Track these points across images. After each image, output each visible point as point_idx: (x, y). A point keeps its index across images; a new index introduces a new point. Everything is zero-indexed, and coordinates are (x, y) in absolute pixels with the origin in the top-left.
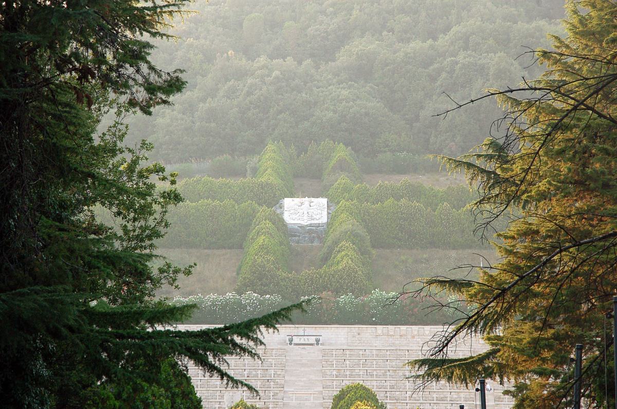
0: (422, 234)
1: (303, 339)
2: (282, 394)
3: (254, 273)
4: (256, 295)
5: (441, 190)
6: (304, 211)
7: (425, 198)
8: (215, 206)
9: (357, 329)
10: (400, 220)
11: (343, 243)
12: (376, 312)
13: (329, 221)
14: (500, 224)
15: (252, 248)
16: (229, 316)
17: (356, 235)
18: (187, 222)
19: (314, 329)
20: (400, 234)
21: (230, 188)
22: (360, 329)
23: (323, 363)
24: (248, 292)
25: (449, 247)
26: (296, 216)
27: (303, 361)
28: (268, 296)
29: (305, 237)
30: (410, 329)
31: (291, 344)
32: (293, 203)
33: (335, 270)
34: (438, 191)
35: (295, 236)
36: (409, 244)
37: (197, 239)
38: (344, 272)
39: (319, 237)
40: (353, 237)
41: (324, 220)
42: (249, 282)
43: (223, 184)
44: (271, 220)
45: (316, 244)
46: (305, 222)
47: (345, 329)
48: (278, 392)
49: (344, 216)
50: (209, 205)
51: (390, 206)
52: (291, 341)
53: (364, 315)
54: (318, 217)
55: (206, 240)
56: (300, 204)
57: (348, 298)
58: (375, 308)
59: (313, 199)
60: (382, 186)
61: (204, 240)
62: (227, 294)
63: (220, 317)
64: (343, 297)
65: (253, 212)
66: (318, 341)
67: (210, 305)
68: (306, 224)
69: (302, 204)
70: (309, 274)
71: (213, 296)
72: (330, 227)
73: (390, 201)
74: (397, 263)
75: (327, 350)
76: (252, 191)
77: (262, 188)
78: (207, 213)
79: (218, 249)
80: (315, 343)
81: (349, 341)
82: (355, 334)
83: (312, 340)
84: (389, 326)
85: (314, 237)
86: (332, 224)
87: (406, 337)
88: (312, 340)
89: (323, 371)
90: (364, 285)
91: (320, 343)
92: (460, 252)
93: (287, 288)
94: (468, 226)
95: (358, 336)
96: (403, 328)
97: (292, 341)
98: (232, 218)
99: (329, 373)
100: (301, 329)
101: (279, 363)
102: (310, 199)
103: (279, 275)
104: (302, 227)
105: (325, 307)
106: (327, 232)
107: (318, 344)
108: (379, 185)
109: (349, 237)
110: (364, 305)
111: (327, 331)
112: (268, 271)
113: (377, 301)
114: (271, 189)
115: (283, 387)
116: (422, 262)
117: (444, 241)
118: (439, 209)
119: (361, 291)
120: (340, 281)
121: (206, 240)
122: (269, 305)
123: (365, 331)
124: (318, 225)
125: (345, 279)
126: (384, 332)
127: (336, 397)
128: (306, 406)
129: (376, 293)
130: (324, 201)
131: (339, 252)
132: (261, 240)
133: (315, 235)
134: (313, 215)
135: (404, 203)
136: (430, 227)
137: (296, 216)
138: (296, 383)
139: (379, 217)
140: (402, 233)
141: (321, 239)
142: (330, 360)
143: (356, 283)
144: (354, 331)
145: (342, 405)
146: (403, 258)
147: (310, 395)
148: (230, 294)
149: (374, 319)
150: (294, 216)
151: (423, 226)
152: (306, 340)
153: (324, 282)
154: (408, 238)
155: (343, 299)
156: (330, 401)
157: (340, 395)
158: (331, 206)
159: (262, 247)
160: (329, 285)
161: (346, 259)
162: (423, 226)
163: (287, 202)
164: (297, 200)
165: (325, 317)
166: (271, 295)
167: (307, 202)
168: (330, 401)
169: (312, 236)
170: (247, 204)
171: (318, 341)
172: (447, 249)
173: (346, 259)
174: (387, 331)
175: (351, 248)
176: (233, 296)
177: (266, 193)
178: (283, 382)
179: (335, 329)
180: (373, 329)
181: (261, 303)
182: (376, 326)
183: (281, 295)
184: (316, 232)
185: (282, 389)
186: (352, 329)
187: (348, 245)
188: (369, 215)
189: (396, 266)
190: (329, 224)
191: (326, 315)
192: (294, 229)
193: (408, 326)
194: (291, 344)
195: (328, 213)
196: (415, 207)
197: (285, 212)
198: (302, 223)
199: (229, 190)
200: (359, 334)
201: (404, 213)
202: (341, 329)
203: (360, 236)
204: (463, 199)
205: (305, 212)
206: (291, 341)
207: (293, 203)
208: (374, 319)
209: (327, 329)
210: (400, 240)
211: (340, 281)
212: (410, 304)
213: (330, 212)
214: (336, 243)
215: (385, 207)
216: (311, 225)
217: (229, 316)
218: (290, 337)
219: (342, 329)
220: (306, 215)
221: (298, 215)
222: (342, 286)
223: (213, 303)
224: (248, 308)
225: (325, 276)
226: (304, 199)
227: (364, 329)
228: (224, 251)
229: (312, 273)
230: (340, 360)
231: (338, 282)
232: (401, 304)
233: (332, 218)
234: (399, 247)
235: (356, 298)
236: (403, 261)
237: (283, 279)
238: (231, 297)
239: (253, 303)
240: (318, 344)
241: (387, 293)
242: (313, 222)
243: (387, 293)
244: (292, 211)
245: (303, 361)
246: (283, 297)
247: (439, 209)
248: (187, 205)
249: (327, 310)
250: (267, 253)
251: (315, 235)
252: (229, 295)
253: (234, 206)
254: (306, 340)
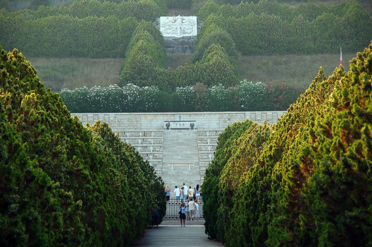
0: (280, 42)
1: (178, 125)
2: (161, 166)
3: (134, 68)
4: (136, 86)
5: (294, 8)
6: (177, 27)
7: (281, 15)
8: (100, 21)
9: (228, 115)
10: (260, 30)
11: (213, 45)
12: (245, 100)
13: (199, 34)
14: (348, 31)
15: (132, 52)
16: (112, 105)
17: (224, 39)
18: (76, 35)
19: (188, 115)
20: (261, 43)
21: (113, 9)
22: (230, 115)
23: (198, 141)
24: (129, 84)
25: (304, 53)
26: (170, 31)
27: (179, 141)
28: (147, 87)
29: (179, 48)
30: (275, 114)
31: (168, 129)
32: (167, 20)
33: (207, 65)
34: (292, 9)
35: (170, 47)
36: (269, 51)
37: (86, 50)
38: (215, 66)
39: (190, 48)
40: (221, 40)
41: (195, 33)
42: (129, 76)
43: (107, 6)
44: (148, 31)
45: (188, 53)
46: (178, 35)
47: (216, 115)
48: (157, 163)
49: (212, 26)
50: (95, 20)
51: (252, 19)
52: (168, 126)
53: (234, 103)
54: (189, 31)
55: (93, 51)
56: (174, 21)
57: (219, 88)
58: (243, 96)
59: (184, 17)
60: (243, 6)
61: (91, 51)
62: (110, 86)
63: (104, 106)
64: (214, 87)
65: (134, 26)
66: (192, 126)
67: (95, 95)
68: (179, 37)
69: (175, 21)
70: (183, 69)
71: (97, 88)
72: (200, 37)
73: (252, 15)
74: (259, 65)
75: (201, 132)
76: (132, 11)
77: (141, 9)
78: (93, 27)
79: (103, 58)
80: (190, 127)
81: (220, 126)
82: (226, 119)
83: (187, 125)
84: (256, 112)
85: (186, 48)
86: (202, 34)
87: (272, 121)
88: (187, 125)
89: (199, 147)
90: (232, 78)
91: (194, 127)
92: (314, 56)
93: (163, 82)
94: (320, 35)
95: (228, 122)
96: (269, 113)
97: (169, 126)
98: (115, 31)
99: (204, 149)
100: (177, 115)
101: (158, 142)
102: (182, 17)
103: (157, 71)
104: (176, 39)
105: (198, 96)
106: (197, 43)
107: (192, 128)
108: (241, 5)
109: (218, 41)
110: (233, 94)
111: (201, 117)
112: (146, 67)
113: (246, 90)
114: (149, 9)
115: (162, 159)
116: (281, 64)
117: (299, 48)
118: (294, 21)
119: (230, 83)
120: (211, 74)
121: (93, 51)
122: (147, 95)
123: (235, 117)
124: (190, 38)
125: (215, 73)
126: (252, 116)
127: (221, 135)
128: (184, 174)
129: (244, 83)
130: (194, 18)
131: (209, 52)
132: (140, 43)
133: (187, 46)
134: (185, 30)
135: (264, 17)
136: (287, 36)
137: (170, 31)
138: (173, 157)
139: (243, 29)
140: (262, 42)
141: (192, 49)
142: (204, 139)
143: (226, 76)
144: (225, 117)
145: (229, 142)
146: (264, 61)
147: (187, 165)
148: (112, 86)
149: (243, 106)
150: (169, 31)
151: (281, 35)
152: (182, 125)
153: (197, 75)
154: (268, 46)
155: (213, 89)
156: (216, 137)
157: (226, 134)
158: (200, 23)
159: (141, 49)
160: (201, 79)
161: (216, 56)
162: (281, 35)
163: (163, 20)
164: (171, 18)
165: (198, 105)
166: (150, 86)
167: (180, 19)
168: (216, 137)
169: (184, 47)
170: (128, 19)
171: (192, 126)
172: (302, 55)
173: (216, 56)
174: (254, 117)
175: (220, 49)
176: (115, 88)
177: (144, 13)
178: (161, 156)
179: (208, 115)
180: (242, 115)
181: (141, 93)
182: (244, 112)
183: (159, 87)
184: (186, 43)
185: (161, 160)
186: (223, 115)
187: (217, 46)
188: (233, 27)
189: (258, 68)
190: (199, 36)
191: (199, 104)
192: (169, 41)
193: (274, 112)
194: (168, 129)
195: (198, 28)
196: (273, 19)
197: (161, 28)
198: (176, 36)
199: (113, 10)
200: (229, 120)
201: (264, 25)
202: (213, 115)
203: (228, 40)
204: (313, 15)
205: (178, 27)
206: (168, 126)
207: (167, 20)
208: (243, 106)
209: (200, 115)
210: (261, 48)
211: (211, 74)
212: (275, 92)
213: (200, 27)
214: (206, 46)
215: (248, 20)
216: (183, 38)
217: (112, 105)
218: (167, 123)
219: (214, 115)
220: (179, 30)
221: (172, 30)
222: (213, 79)
223: (97, 94)
224: (129, 98)
225: (198, 71)
226: (177, 17)
227: (234, 115)
228: (108, 59)
229: (186, 68)
230: (214, 139)
231: (209, 75)
232: (267, 92)
233: (201, 30)
234: (260, 54)
235: (225, 88)
236: (264, 64)
237: (161, 74)
238: (114, 88)
239: (133, 94)
240: (192, 128)
241: (254, 82)
242: (185, 35)
243: (254, 82)
244: (167, 27)
245: (179, 141)
246: (160, 89)
247: (294, 21)
248: (76, 20)
249: (200, 99)
250: (146, 53)
251: (187, 46)
252: (112, 87)
253: (116, 21)
254: (182, 125)
